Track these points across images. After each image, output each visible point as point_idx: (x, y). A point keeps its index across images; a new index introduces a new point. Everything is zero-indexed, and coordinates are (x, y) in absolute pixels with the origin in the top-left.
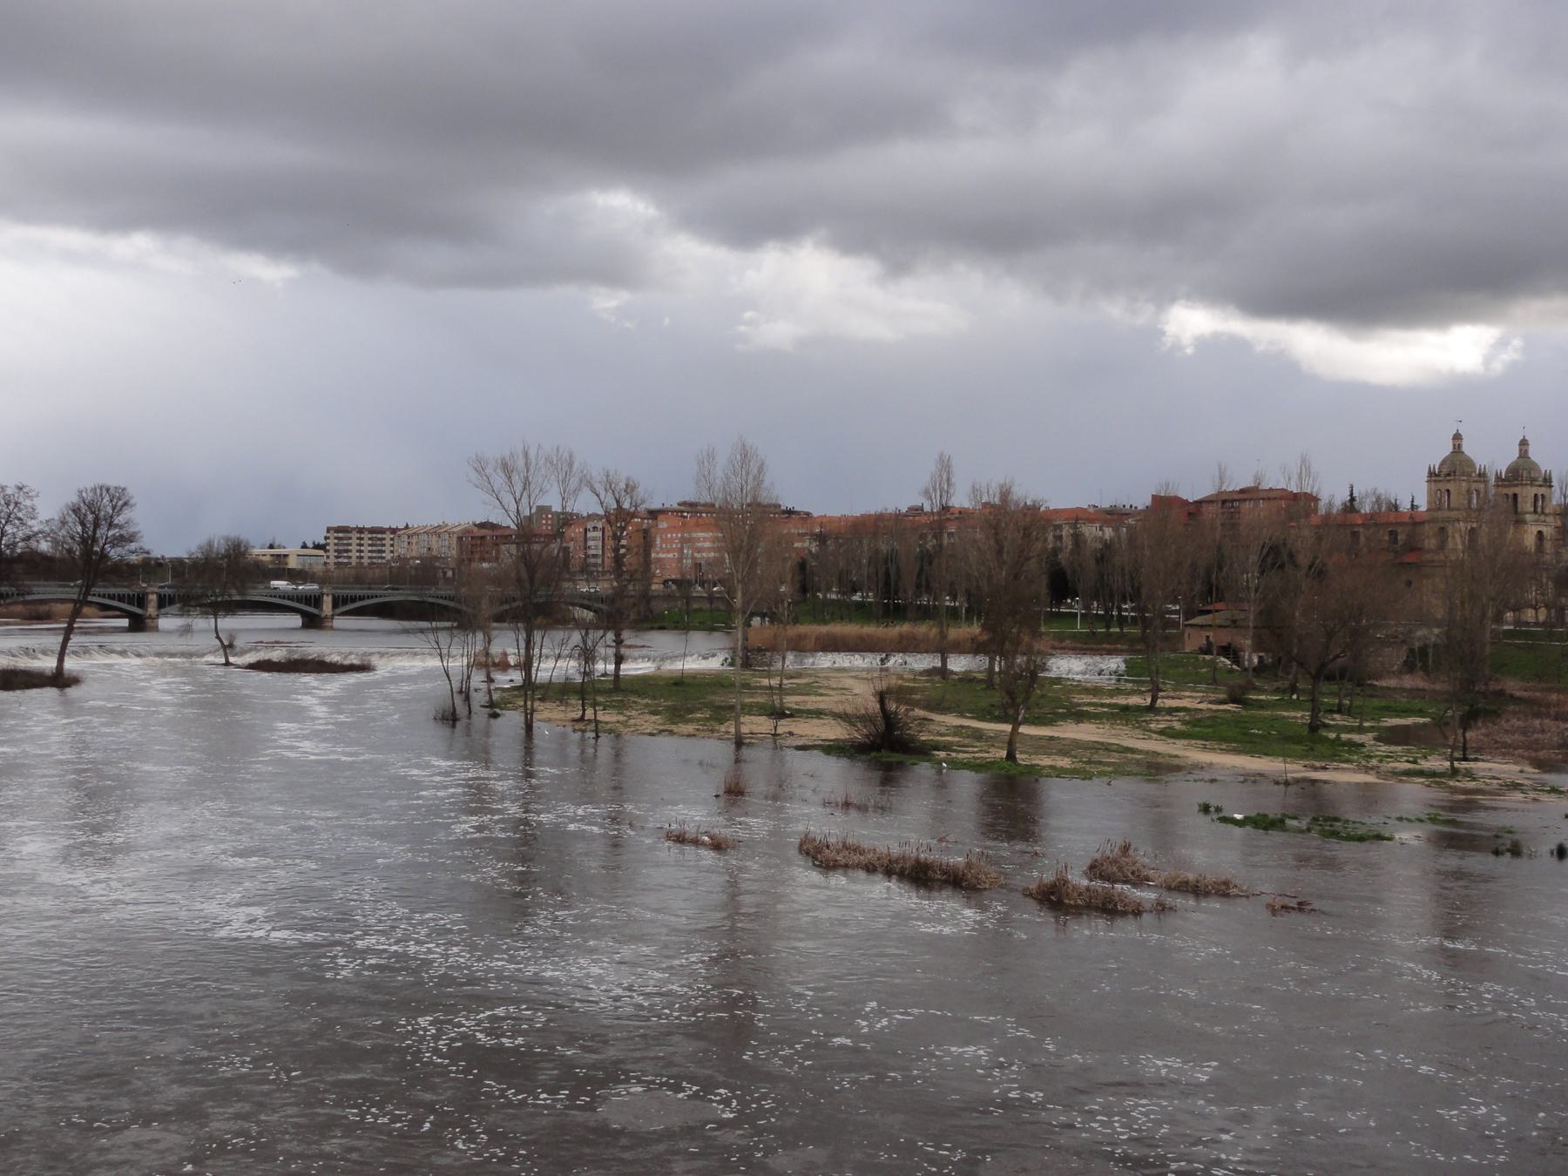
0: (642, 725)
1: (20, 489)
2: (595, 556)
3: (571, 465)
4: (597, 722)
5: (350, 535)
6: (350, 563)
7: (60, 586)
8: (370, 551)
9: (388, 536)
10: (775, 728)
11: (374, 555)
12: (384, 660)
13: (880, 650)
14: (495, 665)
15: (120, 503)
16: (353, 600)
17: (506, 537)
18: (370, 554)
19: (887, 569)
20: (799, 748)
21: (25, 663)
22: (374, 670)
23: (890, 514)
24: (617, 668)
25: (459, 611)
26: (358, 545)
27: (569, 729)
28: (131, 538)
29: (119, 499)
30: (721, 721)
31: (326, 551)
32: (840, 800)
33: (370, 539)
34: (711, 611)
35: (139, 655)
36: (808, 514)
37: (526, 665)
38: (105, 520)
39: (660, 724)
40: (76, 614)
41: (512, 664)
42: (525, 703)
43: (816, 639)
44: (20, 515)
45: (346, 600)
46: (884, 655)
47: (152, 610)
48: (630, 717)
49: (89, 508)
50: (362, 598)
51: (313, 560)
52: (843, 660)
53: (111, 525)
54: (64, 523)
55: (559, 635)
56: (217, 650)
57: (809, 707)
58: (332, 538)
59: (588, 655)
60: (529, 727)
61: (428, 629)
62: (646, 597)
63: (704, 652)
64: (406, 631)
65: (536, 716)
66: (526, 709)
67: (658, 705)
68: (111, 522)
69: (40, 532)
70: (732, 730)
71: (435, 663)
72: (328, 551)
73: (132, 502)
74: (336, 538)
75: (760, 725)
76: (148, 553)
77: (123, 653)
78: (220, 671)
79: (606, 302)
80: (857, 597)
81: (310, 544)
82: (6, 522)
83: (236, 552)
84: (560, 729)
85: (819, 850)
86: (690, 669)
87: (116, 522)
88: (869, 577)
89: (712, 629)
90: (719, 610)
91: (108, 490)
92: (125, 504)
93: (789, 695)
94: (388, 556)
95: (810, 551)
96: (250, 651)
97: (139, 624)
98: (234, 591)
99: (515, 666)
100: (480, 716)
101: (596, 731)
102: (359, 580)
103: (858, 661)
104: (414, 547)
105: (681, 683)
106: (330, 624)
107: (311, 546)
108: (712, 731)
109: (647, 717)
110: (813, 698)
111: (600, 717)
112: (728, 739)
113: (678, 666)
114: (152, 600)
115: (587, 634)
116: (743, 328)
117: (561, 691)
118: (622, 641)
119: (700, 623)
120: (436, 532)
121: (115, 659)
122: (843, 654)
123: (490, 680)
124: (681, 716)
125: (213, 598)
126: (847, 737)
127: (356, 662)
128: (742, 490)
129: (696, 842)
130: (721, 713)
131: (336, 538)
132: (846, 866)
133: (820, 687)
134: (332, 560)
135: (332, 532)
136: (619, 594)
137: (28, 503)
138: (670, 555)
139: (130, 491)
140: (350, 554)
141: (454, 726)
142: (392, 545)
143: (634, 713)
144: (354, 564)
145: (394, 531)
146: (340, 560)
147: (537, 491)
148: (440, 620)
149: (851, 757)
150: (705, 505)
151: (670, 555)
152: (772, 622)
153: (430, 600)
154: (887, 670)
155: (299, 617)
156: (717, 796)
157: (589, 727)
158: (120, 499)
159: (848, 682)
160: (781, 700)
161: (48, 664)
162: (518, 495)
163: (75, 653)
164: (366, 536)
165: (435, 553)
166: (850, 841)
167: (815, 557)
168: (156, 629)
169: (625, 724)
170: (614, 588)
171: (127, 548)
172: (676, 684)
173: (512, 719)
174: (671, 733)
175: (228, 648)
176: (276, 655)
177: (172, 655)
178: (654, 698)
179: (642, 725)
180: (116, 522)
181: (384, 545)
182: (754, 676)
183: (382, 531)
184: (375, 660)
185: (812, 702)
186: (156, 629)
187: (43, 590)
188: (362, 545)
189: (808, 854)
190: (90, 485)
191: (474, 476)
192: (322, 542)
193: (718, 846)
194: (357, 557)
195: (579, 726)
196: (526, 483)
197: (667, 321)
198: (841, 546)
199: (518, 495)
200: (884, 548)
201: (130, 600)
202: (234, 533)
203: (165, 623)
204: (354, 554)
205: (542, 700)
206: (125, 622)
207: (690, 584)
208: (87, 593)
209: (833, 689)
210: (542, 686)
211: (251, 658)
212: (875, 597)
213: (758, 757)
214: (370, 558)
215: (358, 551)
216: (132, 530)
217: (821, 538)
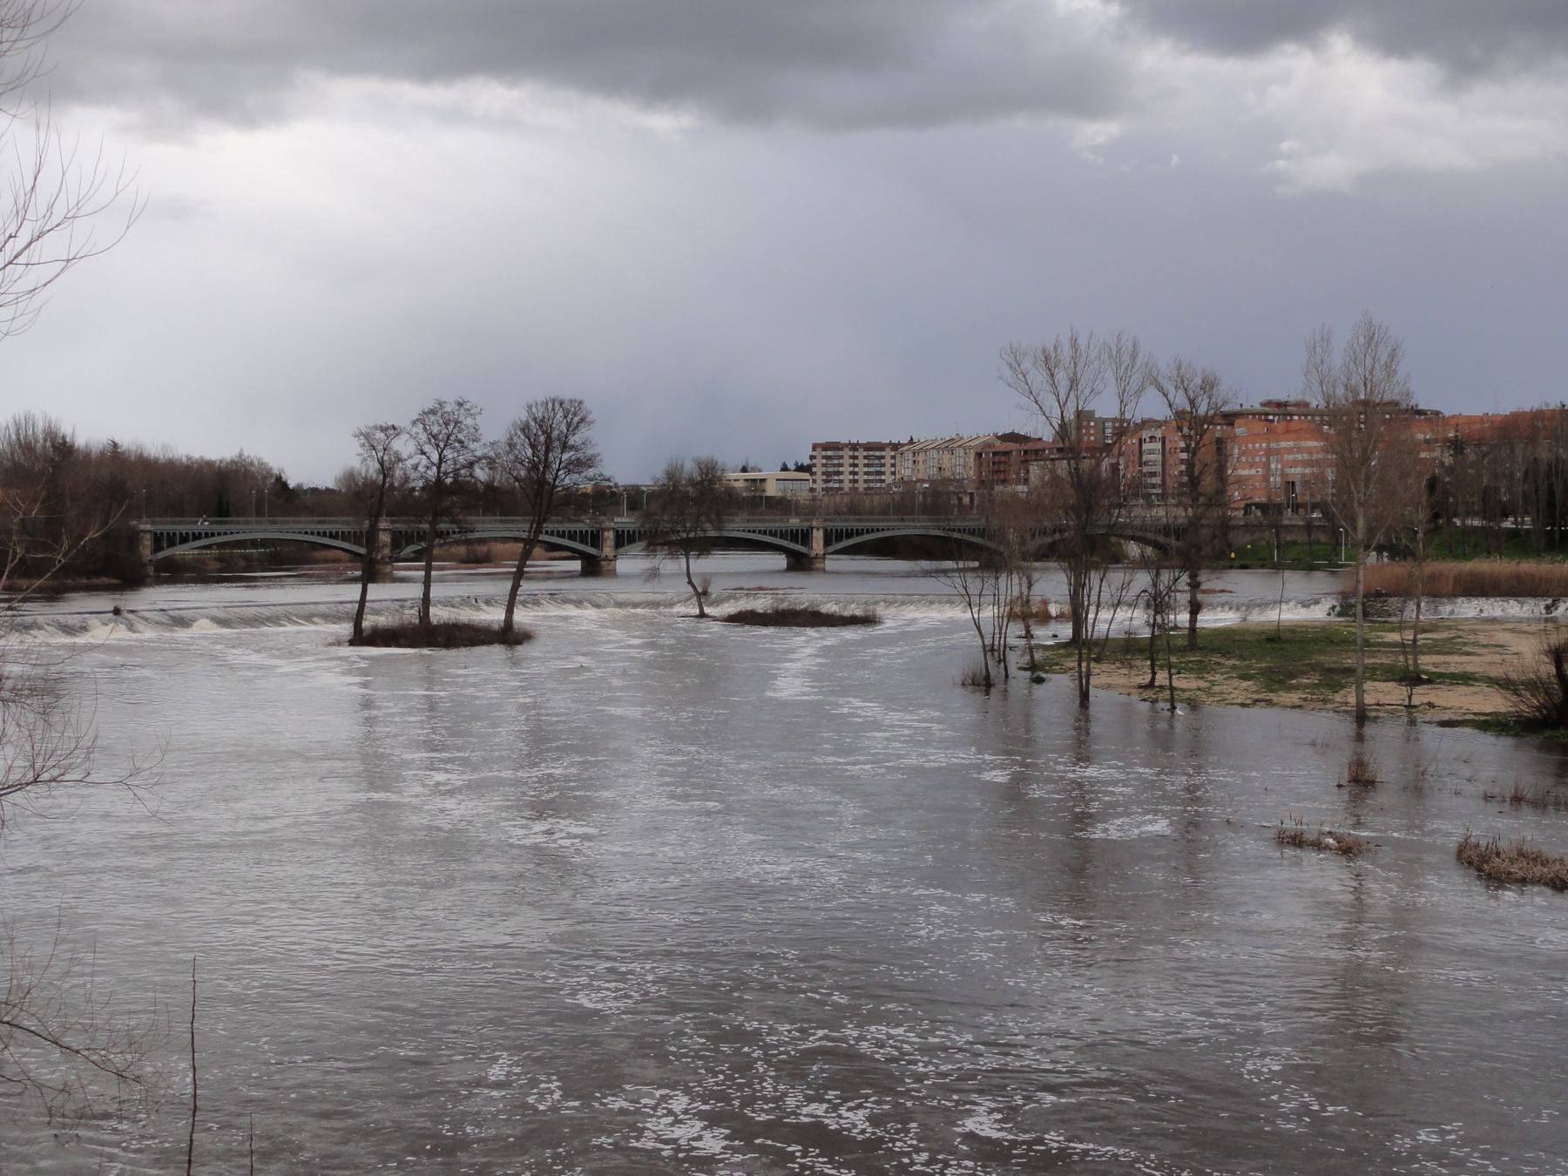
0: (1230, 693)
1: (460, 405)
2: (1153, 474)
3: (1134, 357)
4: (1172, 688)
5: (840, 453)
6: (841, 489)
7: (501, 522)
8: (866, 473)
9: (888, 453)
10: (1410, 697)
11: (871, 478)
12: (892, 610)
13: (1544, 595)
14: (1032, 616)
15: (576, 419)
16: (850, 534)
17: (1036, 452)
18: (866, 477)
19: (1551, 486)
20: (1444, 724)
21: (466, 615)
22: (880, 623)
23: (1553, 410)
24: (1193, 620)
25: (980, 548)
26: (851, 465)
27: (1135, 698)
28: (588, 462)
29: (575, 414)
30: (1336, 687)
31: (813, 474)
32: (1509, 792)
33: (865, 457)
34: (1310, 544)
35: (597, 606)
36: (1437, 413)
37: (1077, 617)
38: (559, 439)
39: (1253, 692)
40: (526, 555)
41: (1054, 613)
42: (1080, 665)
43: (1455, 581)
44: (461, 436)
45: (840, 535)
46: (1549, 601)
47: (608, 549)
48: (1213, 683)
49: (541, 427)
50: (859, 533)
51: (796, 485)
52: (1493, 608)
53: (565, 447)
54: (512, 445)
55: (1116, 577)
56: (688, 600)
57: (1452, 669)
58: (819, 457)
59: (1158, 603)
60: (1084, 697)
61: (953, 570)
62: (1225, 526)
63: (1304, 596)
64: (927, 574)
65: (1093, 680)
66: (1080, 672)
67: (1249, 667)
68: (565, 443)
69: (485, 457)
70: (1352, 700)
71: (959, 613)
72: (815, 473)
73: (590, 418)
74: (824, 457)
75: (1389, 693)
76: (609, 480)
77: (578, 603)
78: (693, 623)
79: (1096, 132)
80: (1508, 524)
81: (791, 466)
82: (445, 446)
83: (709, 476)
84: (1123, 698)
85: (1484, 859)
86: (1259, 623)
87: (571, 442)
88: (1525, 495)
89: (1311, 568)
90: (1318, 542)
91: (561, 404)
92: (582, 420)
93: (1424, 654)
94: (889, 479)
95: (1442, 464)
96: (728, 599)
97: (593, 568)
98: (708, 526)
99: (1057, 616)
100: (1020, 678)
101: (1172, 701)
102: (854, 510)
103: (1514, 609)
104: (921, 466)
105: (1276, 639)
106: (821, 566)
107: (793, 467)
108: (1325, 701)
109: (1236, 683)
110: (1456, 658)
111: (1176, 683)
112: (1346, 712)
113: (1271, 616)
114: (608, 538)
115: (1158, 574)
116: (1281, 164)
117: (1126, 649)
118: (1199, 584)
119: (1294, 560)
120: (949, 446)
121: (571, 611)
122: (1492, 600)
123: (1028, 635)
124: (1280, 682)
125: (684, 535)
126: (1513, 709)
127: (858, 613)
128: (1365, 384)
129: (1318, 846)
130: (1334, 678)
131: (824, 457)
132: (1523, 881)
133: (1465, 644)
134: (820, 485)
135: (819, 449)
136: (1195, 523)
137: (469, 421)
138: (1253, 472)
139: (588, 404)
140: (841, 477)
141: (987, 693)
142: (893, 465)
143: (1217, 677)
144: (846, 490)
145: (896, 447)
146: (830, 485)
147: (1087, 391)
148: (968, 559)
149: (1516, 735)
150: (1297, 405)
151: (1253, 472)
152: (1392, 558)
153: (956, 535)
154: (1554, 620)
155: (783, 556)
156: (1340, 786)
157: (1161, 696)
158: (575, 416)
159: (1504, 638)
160: (1415, 661)
161: (494, 616)
162: (1062, 397)
163: (524, 603)
164: (861, 453)
165: (947, 474)
166: (1527, 848)
167: (1450, 470)
168: (613, 574)
169: (1208, 691)
170: (1187, 516)
171: (584, 474)
172: (1270, 640)
173: (1060, 685)
174: (1269, 703)
175: (702, 595)
176: (761, 604)
177: (636, 605)
178: (1243, 658)
179: (1230, 693)
180: (571, 442)
181: (883, 465)
182: (1373, 629)
183: (880, 447)
184: (880, 610)
185: (1455, 664)
186: (613, 574)
187: (487, 526)
188: (856, 465)
189: (1470, 863)
190: (541, 398)
191: (1007, 372)
192: (807, 462)
193: (1348, 850)
194: (850, 481)
195: (1148, 694)
196: (1074, 383)
197: (1175, 159)
198: (1485, 455)
199: (1062, 397)
200: (1544, 455)
201: (582, 537)
202: (705, 454)
203: (624, 565)
204: (847, 477)
205: (1098, 660)
206: (576, 565)
207: (1279, 509)
208: (538, 531)
209: (1484, 646)
210: (1096, 643)
211: (730, 608)
212: (1533, 522)
213: (1386, 739)
214: (866, 481)
215: (851, 473)
216: (590, 452)
217: (1457, 446)
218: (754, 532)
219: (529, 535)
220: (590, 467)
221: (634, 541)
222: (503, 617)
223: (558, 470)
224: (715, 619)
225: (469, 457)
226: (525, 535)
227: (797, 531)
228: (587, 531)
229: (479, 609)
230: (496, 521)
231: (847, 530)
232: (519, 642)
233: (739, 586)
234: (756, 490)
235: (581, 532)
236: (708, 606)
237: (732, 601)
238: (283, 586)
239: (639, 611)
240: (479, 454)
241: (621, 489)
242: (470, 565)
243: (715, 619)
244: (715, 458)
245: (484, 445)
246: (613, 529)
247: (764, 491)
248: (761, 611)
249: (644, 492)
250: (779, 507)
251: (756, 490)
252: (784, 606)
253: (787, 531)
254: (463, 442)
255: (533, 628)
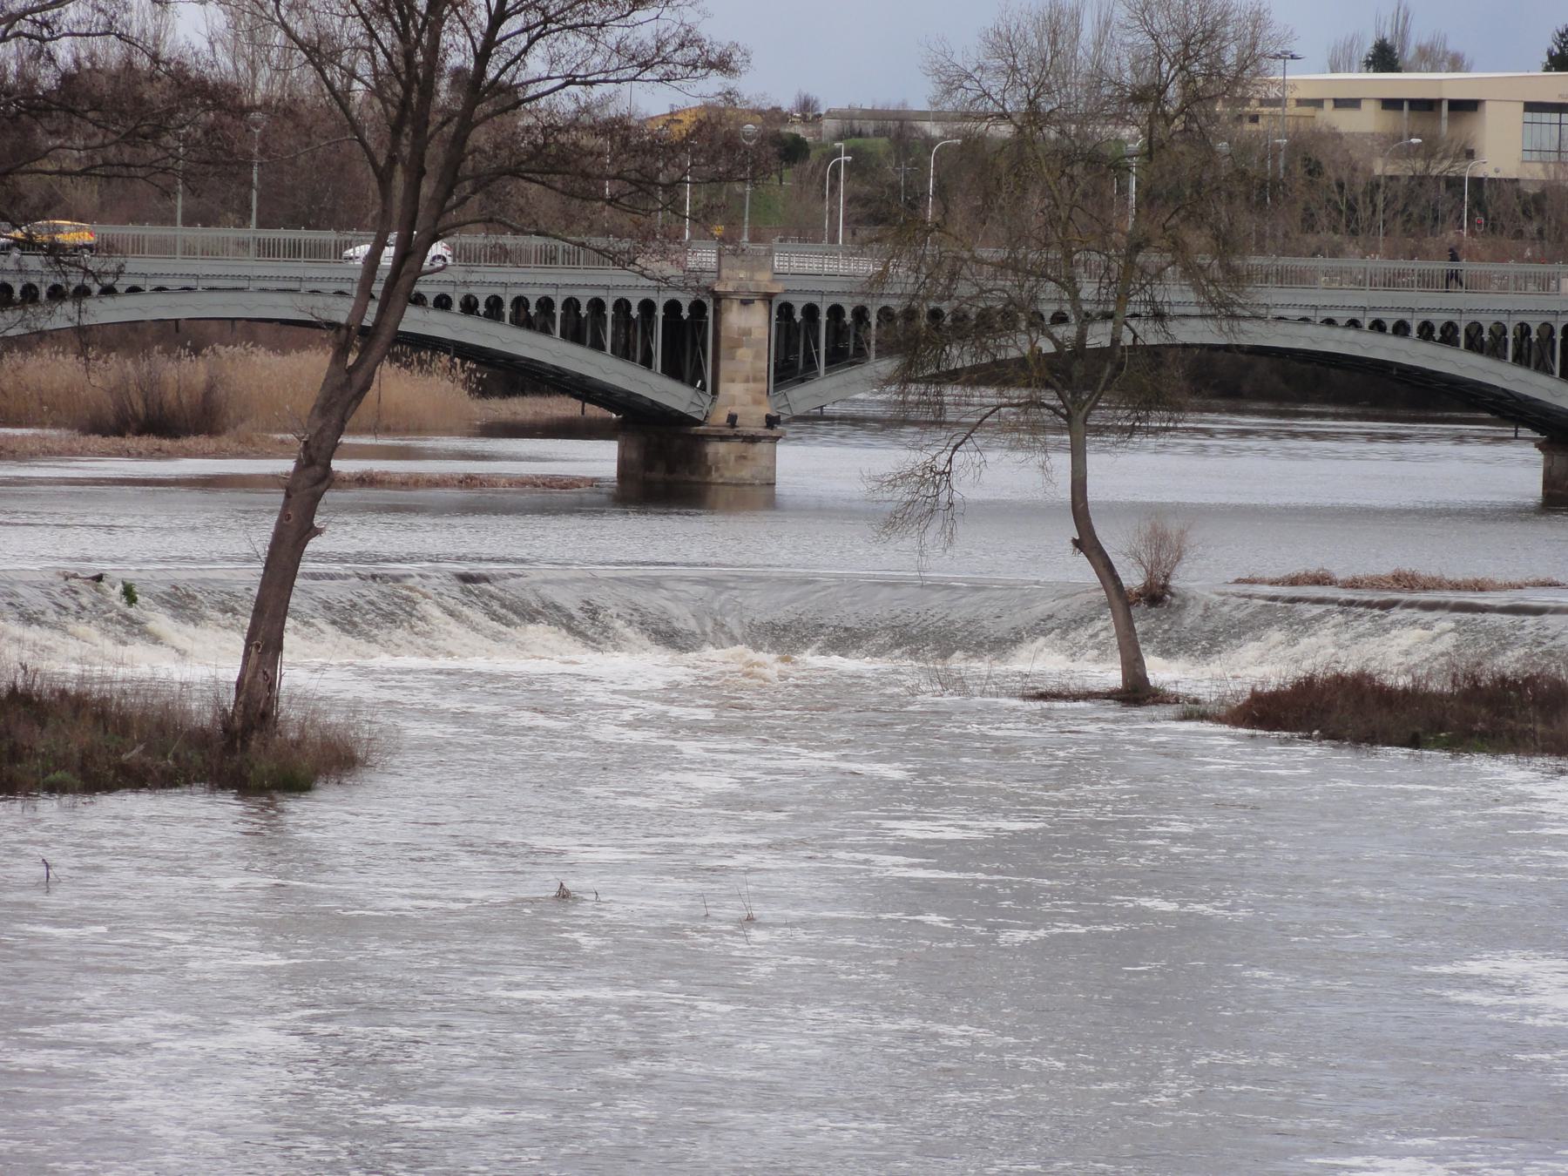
7: (267, 250)
35: (669, 637)
56: (1079, 621)
98: (1176, 293)
171: (613, 35)
218: (1401, 329)
219: (360, 310)
222: (230, 669)
224: (1194, 711)
226: (341, 312)
227: (811, 311)
228: (647, 306)
229: (135, 629)
231: (1524, 329)
232: (297, 784)
233: (1313, 568)
234: (1430, 150)
235: (622, 306)
236: (1166, 653)
237: (1276, 635)
241: (829, 126)
242: (130, 442)
243: (1194, 711)
246: (768, 298)
247: (1470, 154)
248: (1403, 681)
249: (929, 142)
251: (1430, 150)
255: (384, 720)
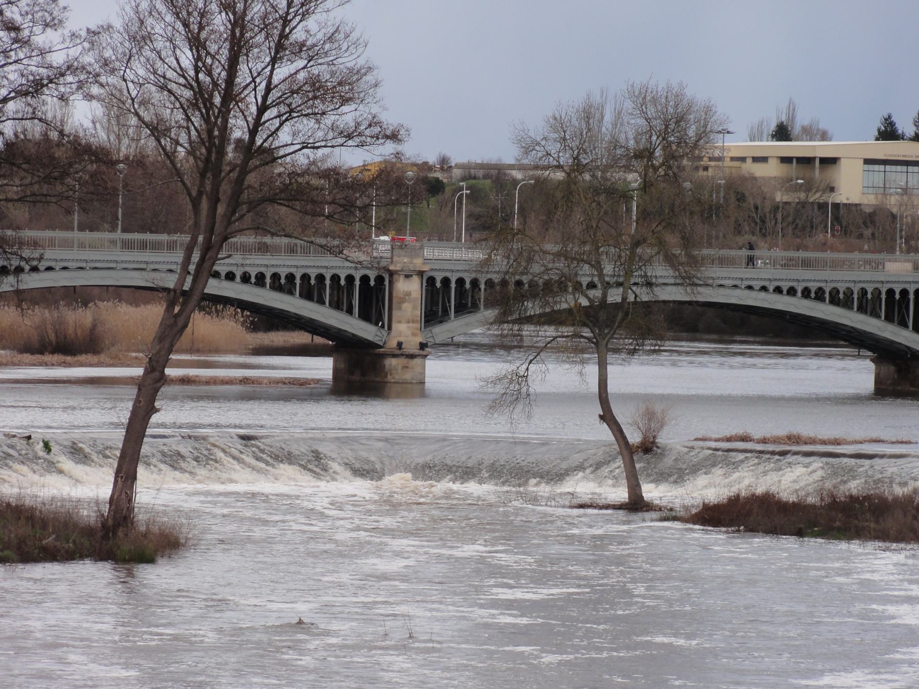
7: (127, 245)
78: (616, 525)
98: (660, 271)
163: (174, 460)
171: (329, 120)
180: (298, 35)
208: (205, 270)
216: (347, 61)
218: (792, 292)
219: (182, 281)
220: (345, 101)
221: (475, 307)
222: (106, 492)
223: (262, 109)
224: (669, 515)
225: (33, 67)
226: (170, 282)
227: (446, 281)
228: (350, 279)
229: (52, 467)
230: (113, 242)
231: (864, 292)
234: (809, 187)
235: (335, 278)
237: (718, 471)
238: (448, 357)
239: (473, 488)
240: (58, 59)
241: (457, 173)
242: (48, 358)
243: (669, 515)
244: (689, 93)
245: (73, 35)
246: (421, 274)
247: (832, 189)
248: (793, 499)
249: (515, 182)
250: (868, 233)
251: (809, 187)
252: (854, 486)
253: (877, 292)
254: (17, 29)
